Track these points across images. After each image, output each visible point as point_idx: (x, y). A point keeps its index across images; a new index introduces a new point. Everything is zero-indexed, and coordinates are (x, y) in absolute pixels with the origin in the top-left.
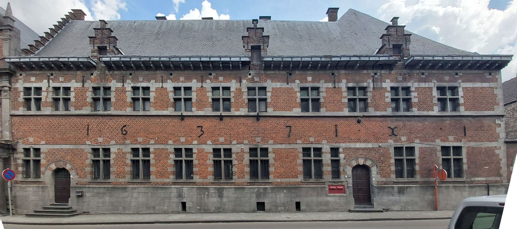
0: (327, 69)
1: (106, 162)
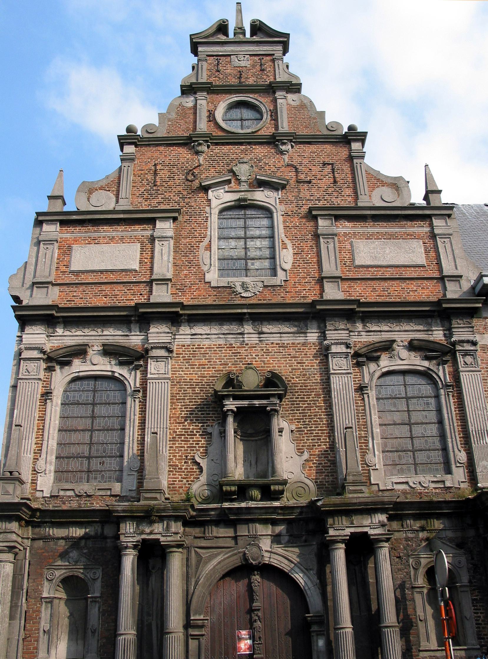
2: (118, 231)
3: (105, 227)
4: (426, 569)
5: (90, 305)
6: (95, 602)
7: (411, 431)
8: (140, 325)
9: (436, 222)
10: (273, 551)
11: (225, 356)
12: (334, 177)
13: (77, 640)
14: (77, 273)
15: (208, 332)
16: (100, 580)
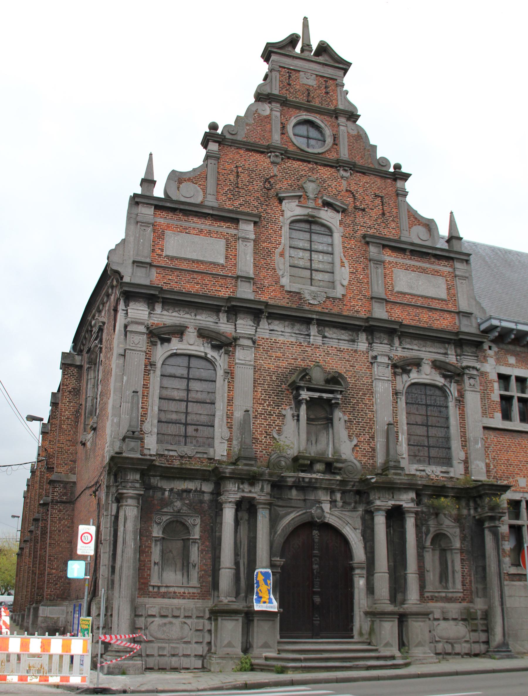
0: (506, 342)
1: (97, 655)
2: (205, 225)
3: (195, 219)
4: (435, 533)
5: (184, 290)
6: (195, 542)
7: (428, 432)
8: (227, 314)
9: (458, 265)
10: (332, 513)
11: (296, 352)
12: (383, 209)
13: (176, 571)
14: (172, 258)
15: (283, 330)
16: (198, 526)
